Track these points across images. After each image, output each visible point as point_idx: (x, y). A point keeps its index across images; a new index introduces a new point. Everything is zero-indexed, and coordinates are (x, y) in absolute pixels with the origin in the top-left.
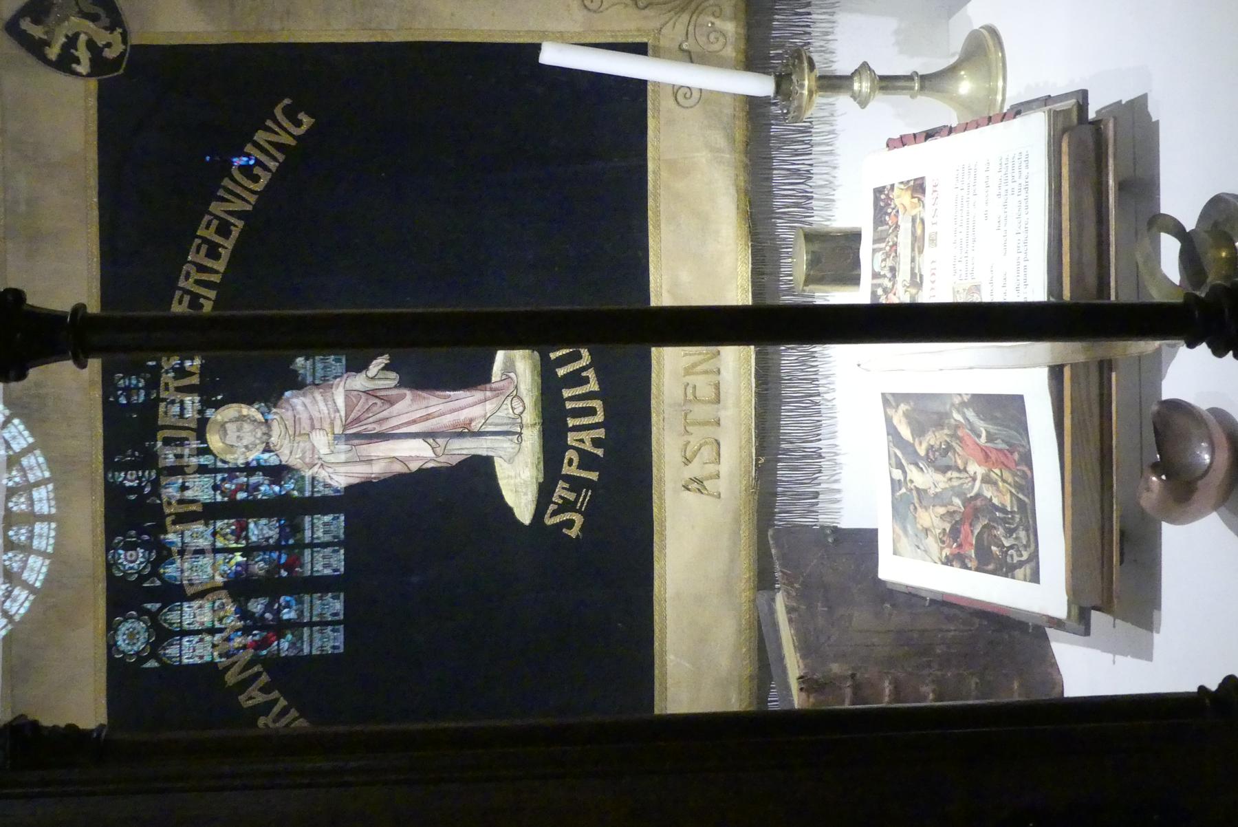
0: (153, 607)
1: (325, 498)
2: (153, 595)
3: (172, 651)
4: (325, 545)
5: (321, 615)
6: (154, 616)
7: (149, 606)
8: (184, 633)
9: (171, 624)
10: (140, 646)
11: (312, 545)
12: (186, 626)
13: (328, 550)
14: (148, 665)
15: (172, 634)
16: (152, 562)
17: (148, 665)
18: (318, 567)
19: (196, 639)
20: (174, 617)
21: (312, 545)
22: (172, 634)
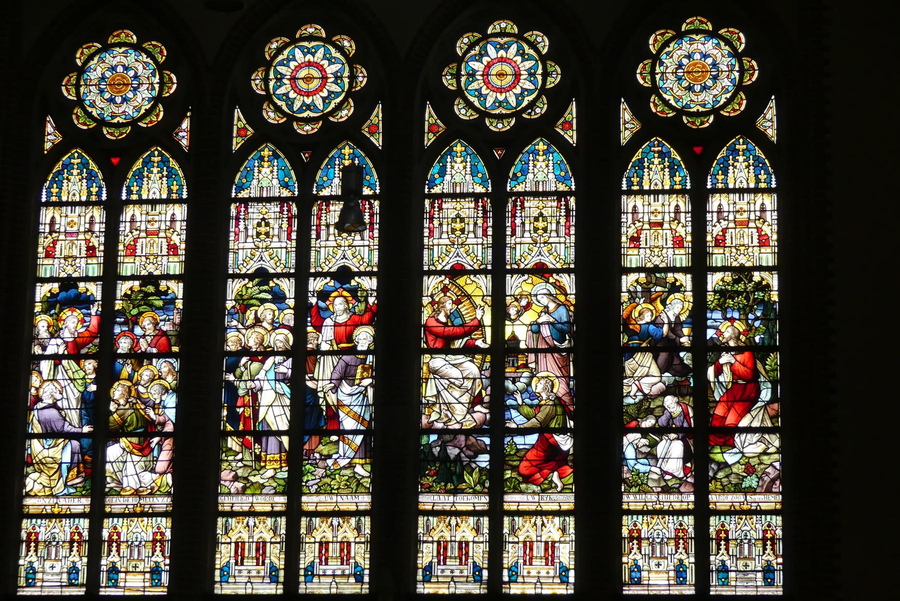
0: (769, 122)
1: (413, 544)
2: (211, 132)
3: (656, 175)
4: (293, 545)
5: (115, 541)
6: (745, 126)
7: (771, 112)
8: (699, 198)
9: (139, 176)
10: (674, 92)
11: (496, 513)
12: (714, 202)
13: (276, 556)
14: (626, 115)
15: (115, 178)
16: (520, 121)
17: (626, 115)
18: (440, 529)
19: (98, 242)
20: (741, 173)
21: (496, 513)
22: (115, 178)
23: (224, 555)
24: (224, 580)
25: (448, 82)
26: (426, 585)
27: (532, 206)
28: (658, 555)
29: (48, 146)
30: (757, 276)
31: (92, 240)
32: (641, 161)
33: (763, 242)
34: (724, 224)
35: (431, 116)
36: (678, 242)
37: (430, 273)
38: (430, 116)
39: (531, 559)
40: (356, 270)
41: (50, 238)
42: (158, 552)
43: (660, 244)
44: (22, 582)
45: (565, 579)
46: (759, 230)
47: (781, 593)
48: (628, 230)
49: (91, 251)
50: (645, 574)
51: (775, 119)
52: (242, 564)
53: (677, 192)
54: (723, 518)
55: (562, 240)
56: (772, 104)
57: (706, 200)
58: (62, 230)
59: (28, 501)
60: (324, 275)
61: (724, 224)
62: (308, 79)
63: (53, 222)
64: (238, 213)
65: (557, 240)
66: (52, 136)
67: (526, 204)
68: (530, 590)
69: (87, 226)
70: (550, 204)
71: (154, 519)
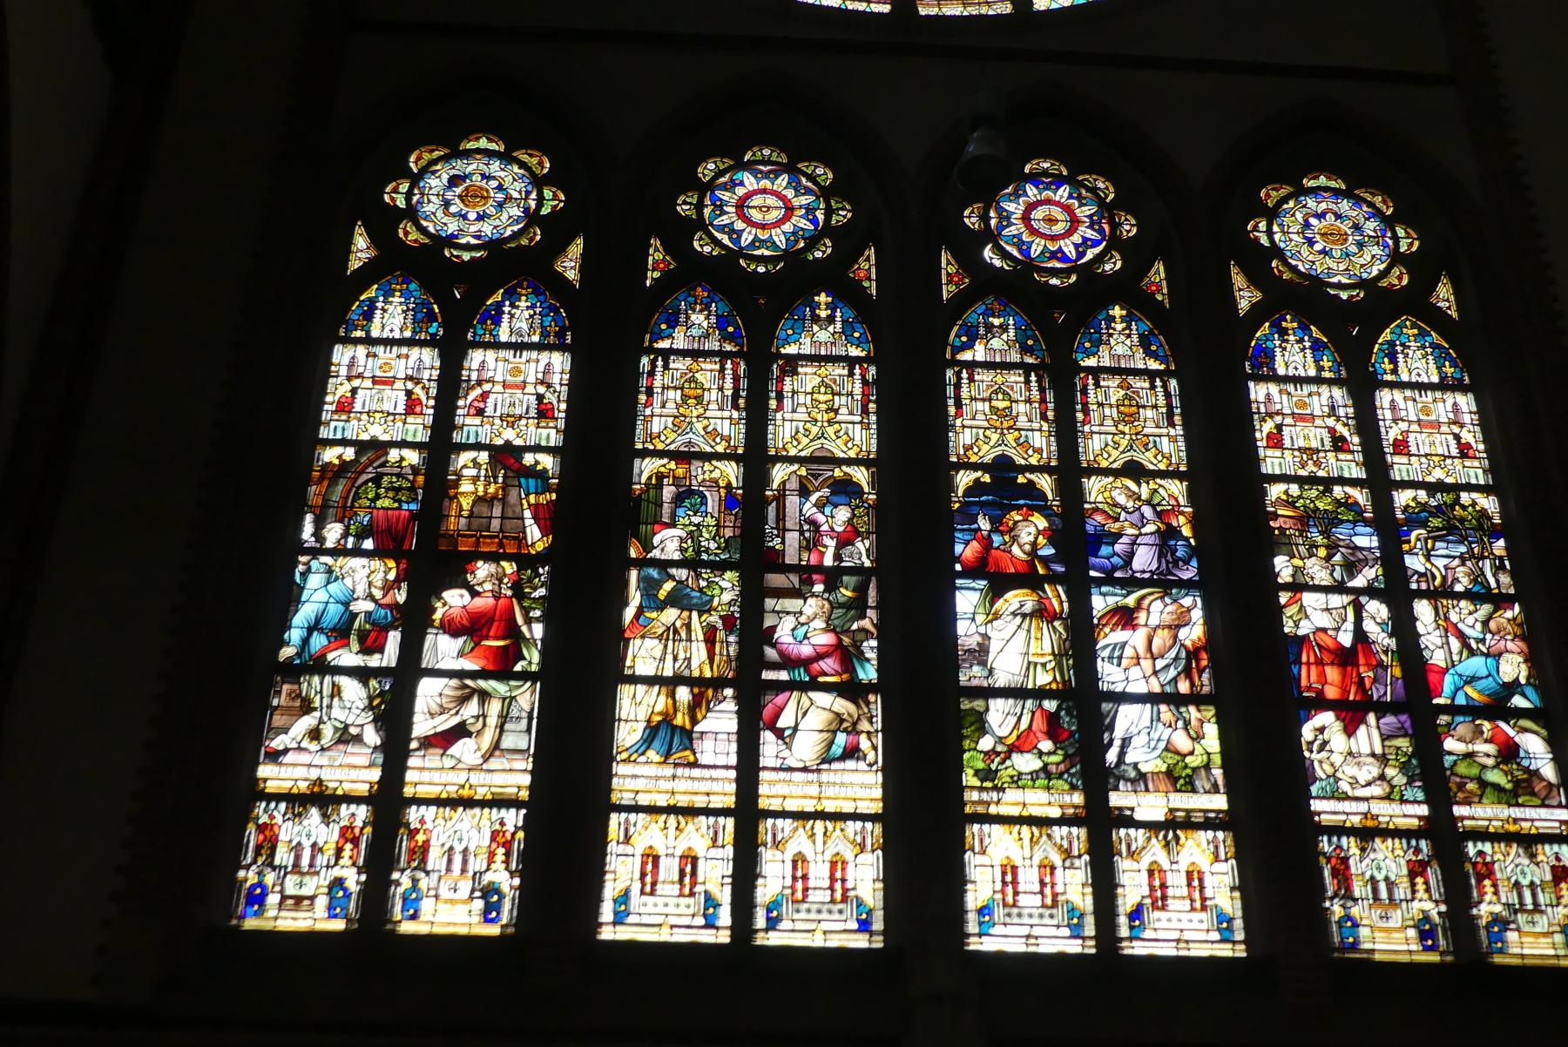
0: (569, 266)
3: (1293, 357)
20: (1419, 364)
23: (621, 871)
24: (772, 924)
25: (971, 220)
26: (618, 928)
27: (809, 377)
28: (1530, 907)
29: (652, 275)
30: (1338, 491)
31: (548, 395)
32: (1392, 344)
33: (544, 413)
34: (1403, 426)
35: (656, 250)
36: (1339, 444)
37: (645, 453)
38: (947, 264)
39: (654, 884)
40: (1023, 462)
41: (347, 387)
42: (1421, 894)
43: (385, 408)
44: (972, 927)
45: (1226, 934)
46: (1457, 437)
47: (728, 940)
48: (338, 389)
49: (412, 406)
50: (1364, 932)
51: (1452, 298)
52: (652, 893)
53: (1330, 382)
54: (273, 805)
55: (1036, 425)
56: (1234, 270)
57: (463, 355)
58: (499, 378)
59: (264, 771)
60: (974, 467)
61: (1403, 426)
62: (1051, 221)
63: (352, 363)
64: (959, 378)
65: (719, 414)
66: (361, 247)
67: (977, 377)
68: (1168, 950)
69: (1451, 416)
70: (709, 366)
71: (486, 811)
